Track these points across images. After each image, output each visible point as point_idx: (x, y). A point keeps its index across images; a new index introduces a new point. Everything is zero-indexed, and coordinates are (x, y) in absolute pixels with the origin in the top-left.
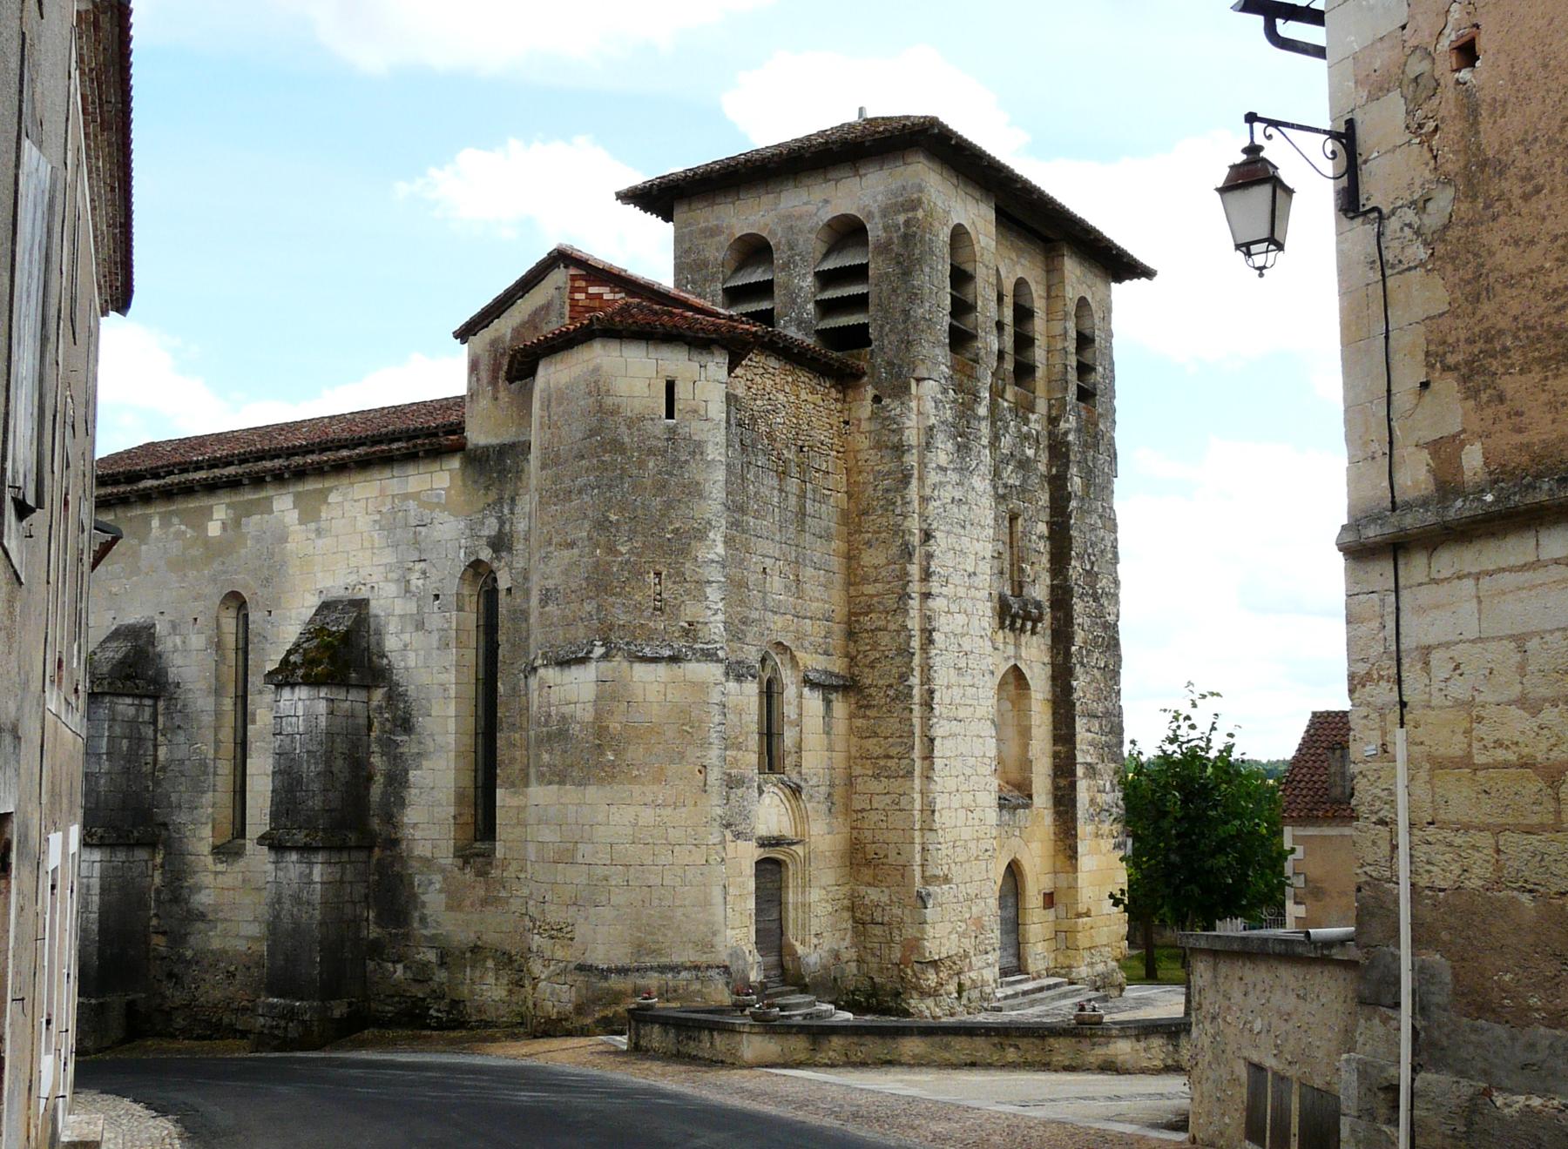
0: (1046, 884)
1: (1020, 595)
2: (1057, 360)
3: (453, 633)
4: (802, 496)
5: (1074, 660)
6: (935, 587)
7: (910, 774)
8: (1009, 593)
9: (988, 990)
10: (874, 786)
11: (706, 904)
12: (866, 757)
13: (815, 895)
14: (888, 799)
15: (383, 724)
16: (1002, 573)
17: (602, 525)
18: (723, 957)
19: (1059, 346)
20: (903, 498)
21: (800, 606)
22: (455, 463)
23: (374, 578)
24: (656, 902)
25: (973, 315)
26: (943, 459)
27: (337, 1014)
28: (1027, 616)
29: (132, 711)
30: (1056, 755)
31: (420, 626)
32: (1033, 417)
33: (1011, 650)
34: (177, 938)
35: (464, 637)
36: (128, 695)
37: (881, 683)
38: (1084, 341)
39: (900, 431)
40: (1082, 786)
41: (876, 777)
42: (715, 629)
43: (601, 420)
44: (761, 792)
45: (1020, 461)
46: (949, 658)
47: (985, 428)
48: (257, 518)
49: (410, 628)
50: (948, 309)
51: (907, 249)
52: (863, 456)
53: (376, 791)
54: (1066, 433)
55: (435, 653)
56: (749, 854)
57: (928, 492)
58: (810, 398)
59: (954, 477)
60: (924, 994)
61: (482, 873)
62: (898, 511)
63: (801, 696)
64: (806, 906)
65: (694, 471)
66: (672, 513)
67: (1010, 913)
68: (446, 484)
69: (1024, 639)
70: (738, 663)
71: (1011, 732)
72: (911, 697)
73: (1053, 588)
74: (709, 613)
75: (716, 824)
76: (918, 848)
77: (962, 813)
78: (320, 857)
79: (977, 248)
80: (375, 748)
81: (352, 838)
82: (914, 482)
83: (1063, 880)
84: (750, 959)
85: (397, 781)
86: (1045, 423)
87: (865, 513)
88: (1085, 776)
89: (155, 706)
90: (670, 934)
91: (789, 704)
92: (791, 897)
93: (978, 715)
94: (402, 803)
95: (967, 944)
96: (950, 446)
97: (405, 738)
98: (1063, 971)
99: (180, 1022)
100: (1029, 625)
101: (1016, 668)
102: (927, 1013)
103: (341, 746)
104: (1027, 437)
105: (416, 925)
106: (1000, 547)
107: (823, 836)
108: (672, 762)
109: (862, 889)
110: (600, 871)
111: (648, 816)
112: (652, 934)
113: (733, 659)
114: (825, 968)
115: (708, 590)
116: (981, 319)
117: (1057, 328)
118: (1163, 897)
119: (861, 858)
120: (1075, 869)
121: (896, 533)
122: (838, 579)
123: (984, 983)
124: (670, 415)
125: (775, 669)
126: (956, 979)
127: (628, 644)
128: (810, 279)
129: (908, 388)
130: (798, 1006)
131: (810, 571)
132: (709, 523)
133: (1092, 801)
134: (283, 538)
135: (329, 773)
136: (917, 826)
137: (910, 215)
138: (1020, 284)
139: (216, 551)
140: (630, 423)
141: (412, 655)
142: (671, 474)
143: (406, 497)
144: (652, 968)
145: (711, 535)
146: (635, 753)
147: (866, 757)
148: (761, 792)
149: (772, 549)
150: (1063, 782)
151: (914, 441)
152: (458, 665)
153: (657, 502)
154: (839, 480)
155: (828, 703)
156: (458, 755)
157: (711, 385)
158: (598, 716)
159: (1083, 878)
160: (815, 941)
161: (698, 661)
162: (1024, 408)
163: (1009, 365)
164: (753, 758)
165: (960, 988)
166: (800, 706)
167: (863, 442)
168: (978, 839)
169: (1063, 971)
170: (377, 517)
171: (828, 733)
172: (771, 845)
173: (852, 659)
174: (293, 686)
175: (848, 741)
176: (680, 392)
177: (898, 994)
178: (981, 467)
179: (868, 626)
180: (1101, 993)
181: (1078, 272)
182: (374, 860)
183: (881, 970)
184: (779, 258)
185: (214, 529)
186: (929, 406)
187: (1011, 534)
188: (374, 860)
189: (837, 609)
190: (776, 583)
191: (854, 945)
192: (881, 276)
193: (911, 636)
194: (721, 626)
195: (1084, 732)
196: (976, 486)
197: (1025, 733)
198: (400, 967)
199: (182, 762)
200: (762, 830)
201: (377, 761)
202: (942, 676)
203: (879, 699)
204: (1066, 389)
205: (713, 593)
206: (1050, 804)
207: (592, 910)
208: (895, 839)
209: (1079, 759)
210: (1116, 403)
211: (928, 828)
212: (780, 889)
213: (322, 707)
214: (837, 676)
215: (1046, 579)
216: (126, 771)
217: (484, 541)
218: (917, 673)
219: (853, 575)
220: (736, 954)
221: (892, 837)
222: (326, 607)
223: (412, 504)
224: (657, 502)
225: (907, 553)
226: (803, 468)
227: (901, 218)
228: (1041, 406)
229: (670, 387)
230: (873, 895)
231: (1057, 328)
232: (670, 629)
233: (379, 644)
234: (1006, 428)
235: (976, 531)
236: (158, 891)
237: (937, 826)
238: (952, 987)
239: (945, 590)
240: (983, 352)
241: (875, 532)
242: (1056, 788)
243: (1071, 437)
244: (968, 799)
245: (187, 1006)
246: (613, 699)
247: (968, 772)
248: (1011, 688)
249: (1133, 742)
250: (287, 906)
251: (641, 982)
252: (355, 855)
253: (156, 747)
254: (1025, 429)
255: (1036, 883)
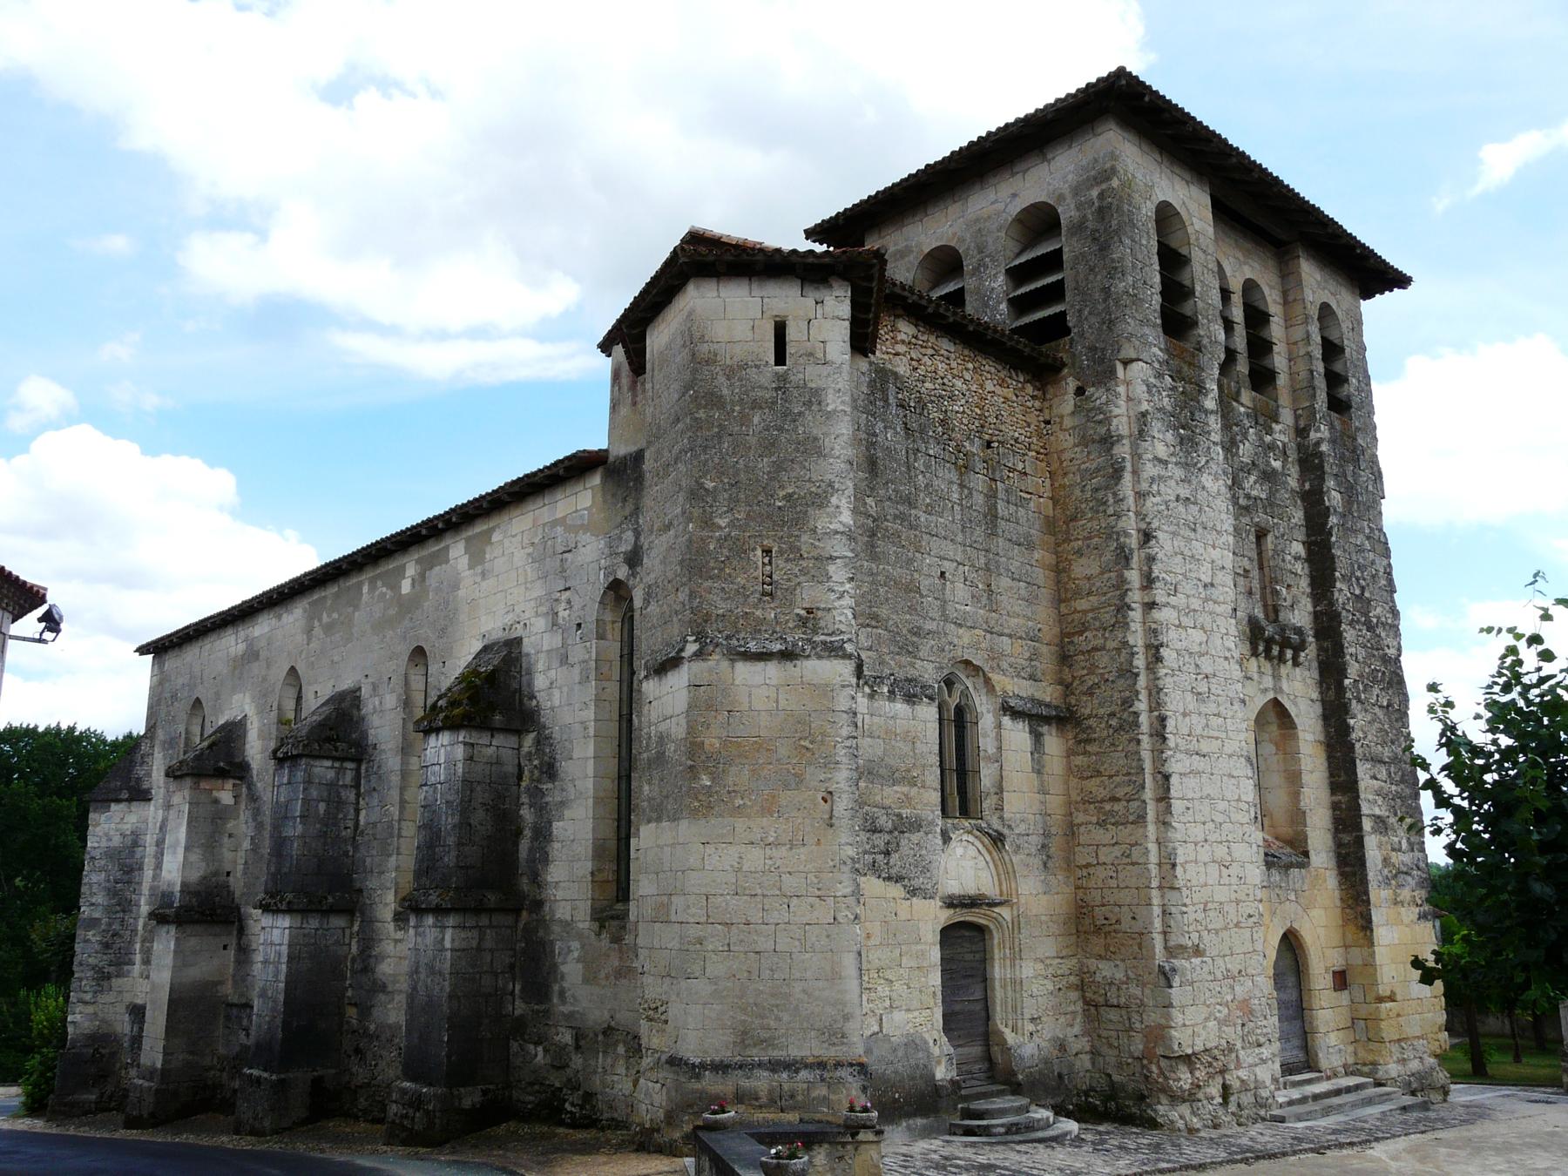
0: (1336, 960)
1: (1276, 620)
2: (1301, 367)
3: (593, 664)
4: (992, 495)
5: (1349, 695)
6: (1160, 595)
7: (1141, 819)
8: (1261, 616)
9: (1264, 1093)
10: (1100, 836)
11: (835, 976)
12: (1088, 801)
13: (1028, 970)
14: (1117, 851)
15: (532, 772)
16: (1250, 593)
17: (696, 494)
18: (857, 1051)
19: (1302, 352)
20: (1115, 494)
21: (990, 614)
22: (596, 479)
23: (527, 615)
24: (766, 974)
25: (1191, 302)
26: (1161, 450)
27: (467, 1103)
28: (1285, 644)
29: (331, 774)
30: (1335, 806)
31: (564, 660)
32: (1277, 427)
33: (1268, 682)
34: (365, 1011)
35: (605, 669)
36: (327, 758)
37: (1101, 711)
38: (1332, 350)
39: (1107, 420)
40: (1372, 843)
41: (1101, 824)
42: (842, 614)
43: (694, 371)
44: (946, 838)
45: (1264, 472)
46: (1185, 679)
47: (1214, 423)
48: (437, 569)
49: (555, 664)
50: (1158, 288)
51: (1106, 218)
52: (1067, 456)
53: (524, 845)
54: (1318, 444)
55: (577, 687)
56: (931, 917)
57: (1144, 486)
58: (998, 390)
59: (1179, 473)
60: (1176, 1098)
61: (616, 939)
62: (1111, 511)
63: (999, 726)
64: (1017, 984)
65: (811, 424)
66: (784, 476)
67: (1291, 995)
68: (589, 503)
69: (1285, 669)
70: (909, 680)
71: (1276, 780)
72: (1137, 725)
73: (1316, 616)
74: (833, 596)
75: (846, 869)
76: (1157, 911)
77: (1213, 870)
78: (451, 920)
79: (1190, 230)
80: (524, 799)
81: (492, 898)
82: (1127, 477)
83: (1357, 956)
84: (936, 1051)
85: (543, 834)
86: (1293, 435)
87: (1074, 519)
88: (1374, 831)
89: (358, 770)
90: (786, 1017)
91: (985, 735)
92: (998, 971)
93: (1228, 749)
94: (546, 860)
95: (1232, 1034)
96: (1169, 436)
97: (550, 786)
98: (1366, 1068)
99: (363, 1102)
100: (1289, 653)
101: (1276, 703)
102: (1180, 1124)
103: (481, 795)
104: (1271, 447)
105: (555, 1001)
106: (1246, 563)
107: (1036, 897)
108: (786, 787)
109: (1092, 963)
110: (694, 932)
111: (755, 858)
112: (762, 1017)
113: (901, 675)
114: (1047, 1061)
115: (831, 569)
116: (1200, 304)
117: (1298, 333)
118: (1525, 967)
119: (1091, 926)
120: (1371, 944)
121: (1109, 537)
122: (1045, 594)
123: (1259, 1085)
124: (780, 359)
125: (965, 694)
126: (1219, 1080)
127: (728, 638)
128: (1001, 278)
129: (1113, 372)
130: (1002, 1112)
131: (1005, 582)
132: (831, 484)
133: (1386, 861)
134: (455, 587)
135: (465, 825)
136: (1154, 884)
137: (1104, 186)
138: (1250, 287)
139: (408, 606)
140: (730, 372)
141: (556, 693)
142: (781, 429)
143: (554, 524)
144: (760, 1065)
145: (834, 500)
146: (738, 776)
147: (1088, 801)
148: (946, 838)
149: (950, 550)
150: (1346, 838)
151: (1124, 430)
152: (598, 700)
153: (765, 464)
154: (1038, 482)
155: (1037, 737)
156: (598, 801)
157: (828, 324)
158: (691, 730)
159: (1382, 954)
160: (1031, 1027)
161: (820, 657)
162: (1266, 417)
163: (1242, 367)
164: (935, 797)
165: (1226, 1091)
166: (999, 738)
167: (1066, 441)
168: (1238, 902)
169: (1366, 1068)
170: (530, 550)
171: (1039, 772)
172: (963, 906)
173: (1067, 686)
174: (438, 731)
175: (1066, 782)
176: (792, 334)
177: (1142, 1098)
178: (1211, 464)
179: (1084, 647)
180: (1419, 1099)
181: (1318, 277)
182: (521, 925)
183: (1120, 1066)
184: (968, 266)
185: (406, 587)
186: (1140, 390)
187: (1260, 554)
188: (521, 925)
189: (1045, 628)
190: (959, 591)
191: (1086, 1033)
192: (1076, 257)
193: (1133, 654)
194: (849, 613)
195: (1368, 780)
196: (1207, 485)
197: (1294, 779)
198: (540, 1049)
199: (374, 824)
200: (953, 887)
201: (527, 814)
202: (1175, 702)
203: (1100, 731)
204: (1314, 396)
205: (838, 573)
206: (1332, 864)
207: (684, 984)
208: (1128, 900)
209: (1365, 809)
210: (1376, 419)
211: (1168, 885)
212: (984, 961)
213: (460, 752)
214: (1048, 706)
215: (1306, 605)
216: (323, 835)
217: (621, 559)
218: (1143, 696)
219: (1063, 590)
220: (914, 1044)
221: (1125, 897)
222: (485, 649)
223: (559, 529)
224: (765, 464)
225: (1123, 557)
226: (992, 467)
227: (1095, 193)
228: (1287, 416)
229: (780, 330)
230: (1105, 970)
231: (1298, 333)
232: (782, 618)
233: (530, 684)
234: (1245, 435)
235: (1211, 537)
236: (354, 960)
237: (1180, 883)
238: (1214, 1090)
239: (1173, 600)
240: (1205, 341)
241: (1086, 538)
242: (1339, 845)
243: (1324, 448)
244: (1221, 852)
245: (368, 1085)
246: (709, 707)
247: (1219, 818)
248: (1274, 729)
249: (1433, 688)
250: (422, 976)
251: (746, 1084)
252: (499, 919)
253: (357, 811)
254: (1268, 439)
255: (1322, 957)
